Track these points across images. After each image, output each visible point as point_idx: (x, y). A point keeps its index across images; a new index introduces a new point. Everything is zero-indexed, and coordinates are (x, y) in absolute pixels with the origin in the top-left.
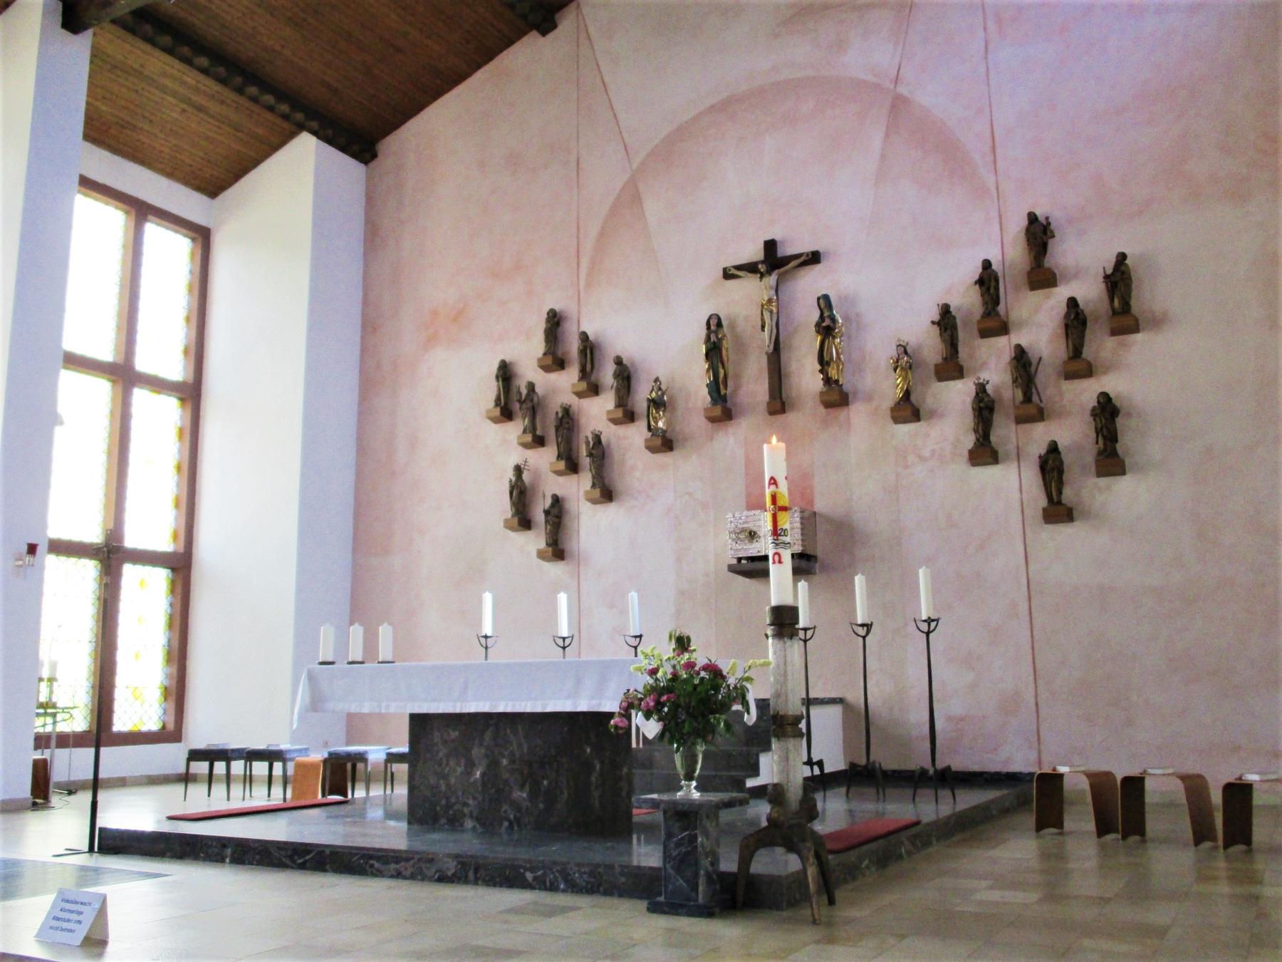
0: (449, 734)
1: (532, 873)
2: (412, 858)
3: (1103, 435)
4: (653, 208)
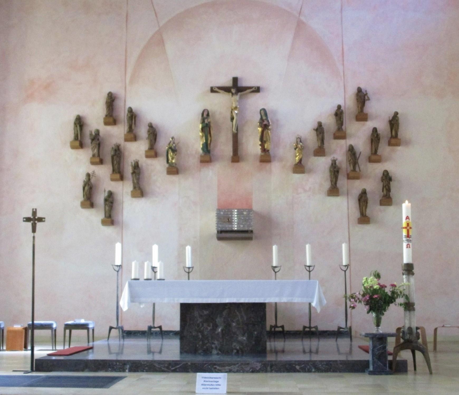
0: (203, 312)
1: (299, 366)
2: (238, 364)
3: (386, 188)
4: (170, 48)
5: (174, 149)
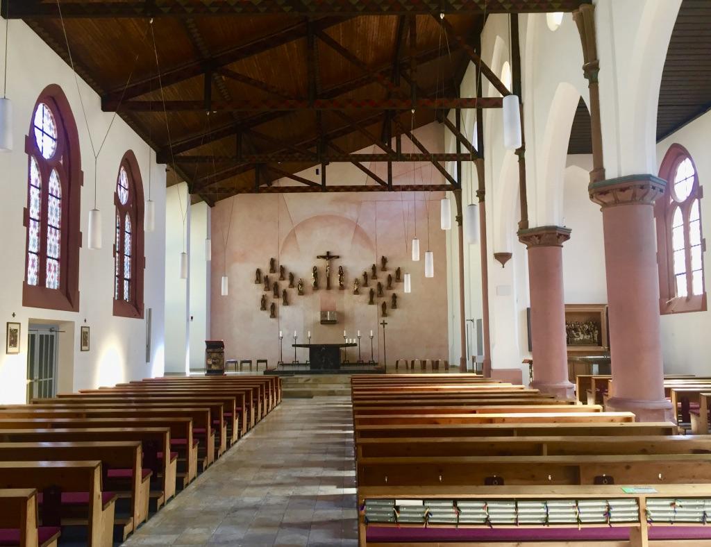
4: (300, 236)
5: (302, 284)
